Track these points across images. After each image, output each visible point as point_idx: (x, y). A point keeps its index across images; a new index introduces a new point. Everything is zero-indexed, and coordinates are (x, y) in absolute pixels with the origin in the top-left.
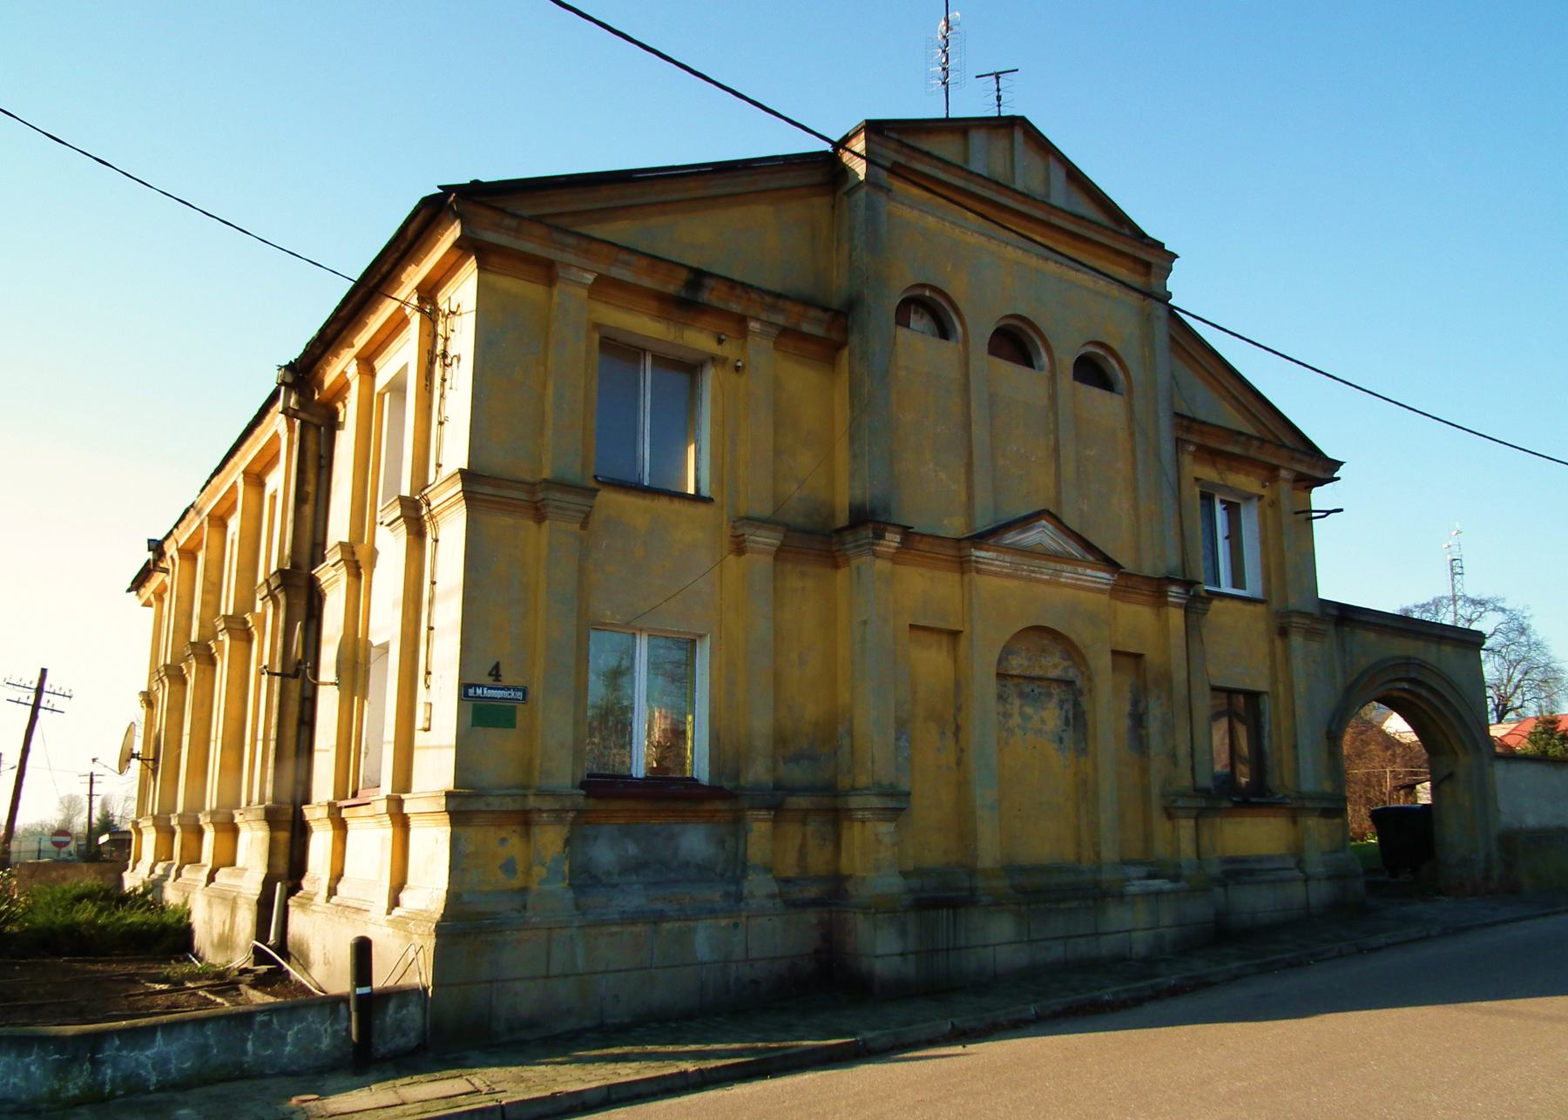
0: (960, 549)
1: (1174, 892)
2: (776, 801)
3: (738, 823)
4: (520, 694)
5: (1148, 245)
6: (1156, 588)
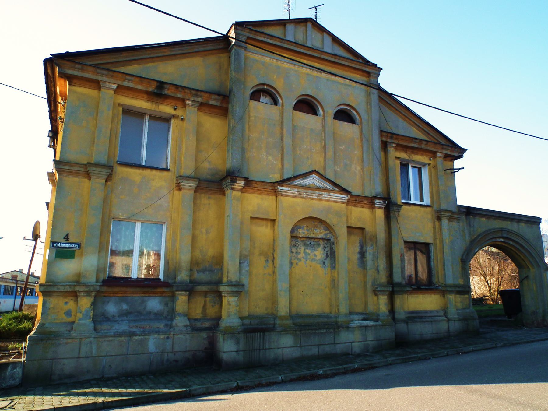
0: (275, 187)
1: (373, 326)
2: (190, 288)
3: (173, 298)
4: (77, 246)
5: (370, 65)
6: (370, 201)
